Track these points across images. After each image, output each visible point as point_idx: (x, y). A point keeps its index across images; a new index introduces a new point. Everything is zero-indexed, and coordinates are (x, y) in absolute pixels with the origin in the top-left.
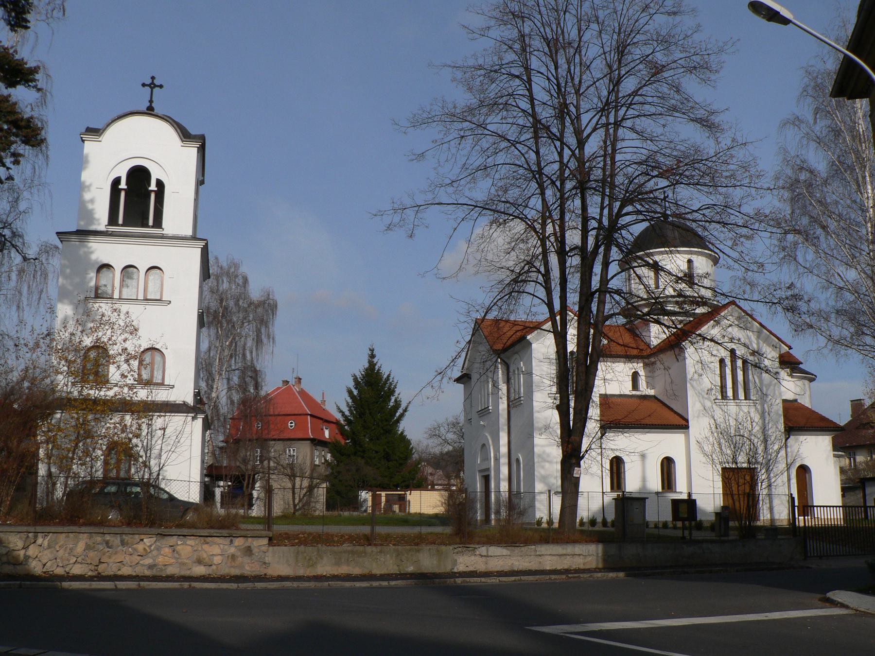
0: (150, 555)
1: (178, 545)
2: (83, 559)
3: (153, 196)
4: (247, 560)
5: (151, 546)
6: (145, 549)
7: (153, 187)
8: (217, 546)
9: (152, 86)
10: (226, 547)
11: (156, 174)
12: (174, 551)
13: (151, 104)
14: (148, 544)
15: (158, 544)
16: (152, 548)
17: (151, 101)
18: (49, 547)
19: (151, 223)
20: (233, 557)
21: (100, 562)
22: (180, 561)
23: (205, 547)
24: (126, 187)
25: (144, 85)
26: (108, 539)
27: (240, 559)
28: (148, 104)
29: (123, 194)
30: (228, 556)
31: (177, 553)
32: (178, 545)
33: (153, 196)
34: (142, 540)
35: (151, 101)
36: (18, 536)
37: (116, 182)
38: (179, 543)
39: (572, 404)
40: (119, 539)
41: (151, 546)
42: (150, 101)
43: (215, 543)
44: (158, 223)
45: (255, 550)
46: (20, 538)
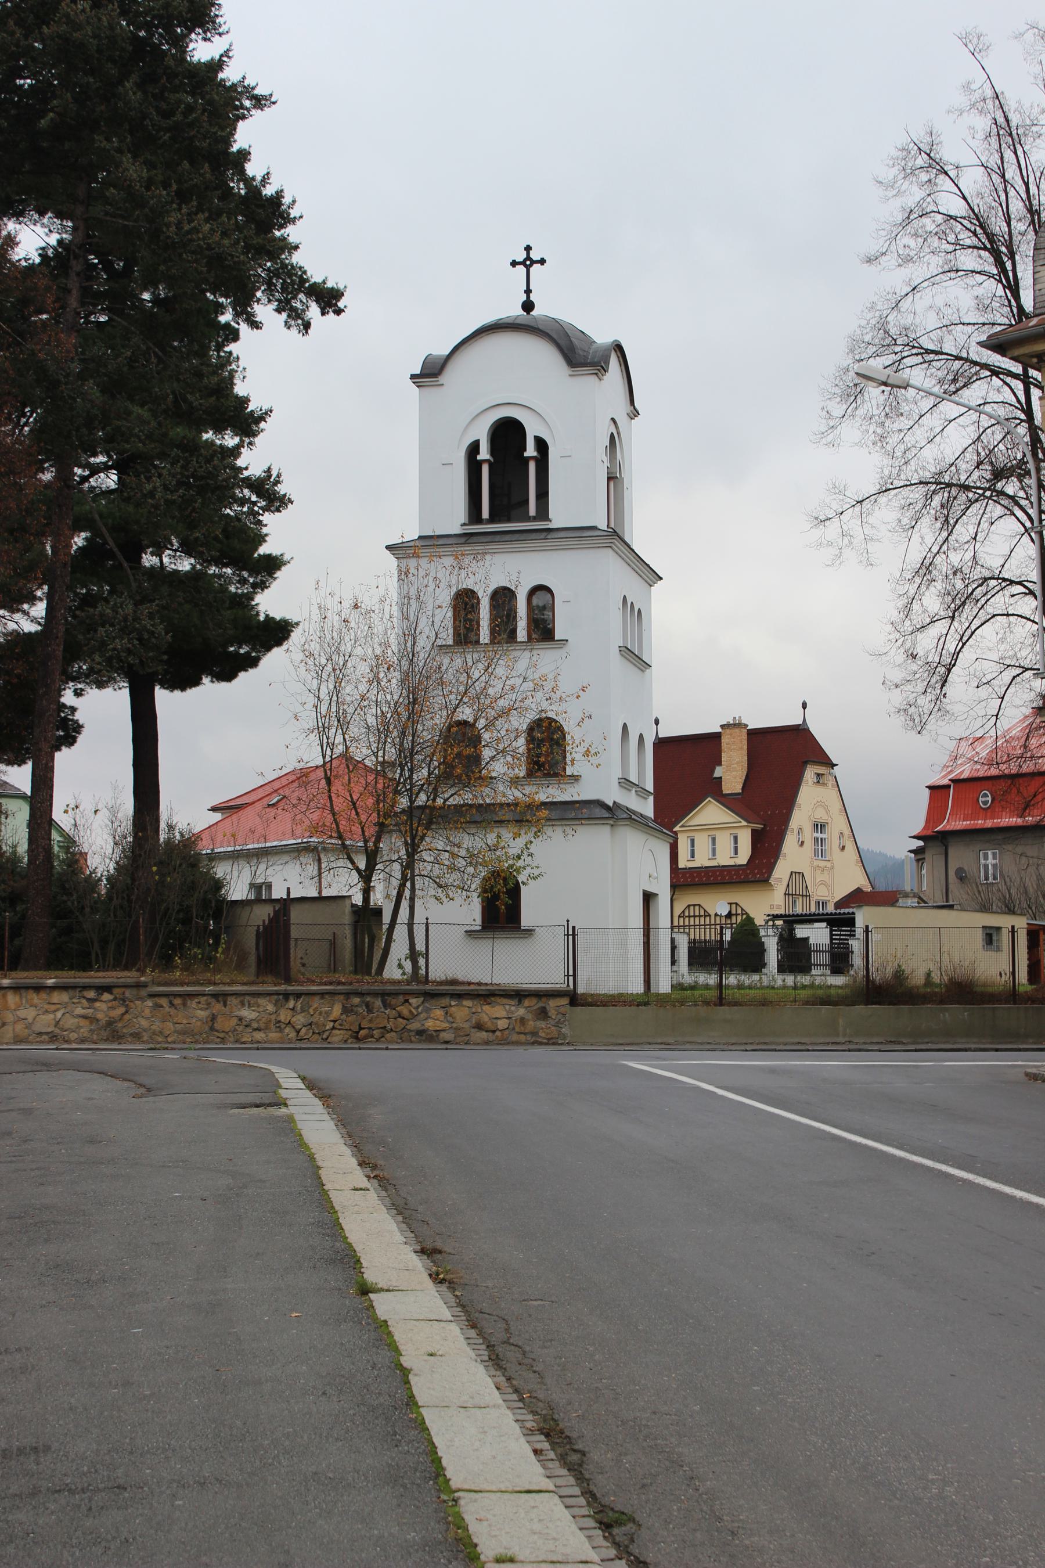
0: (418, 1018)
1: (451, 1006)
2: (341, 1025)
3: (532, 466)
4: (542, 1024)
5: (418, 1007)
6: (411, 1011)
7: (531, 451)
8: (502, 1007)
9: (528, 263)
10: (513, 1008)
11: (532, 430)
12: (446, 1013)
13: (528, 297)
14: (414, 1005)
15: (427, 1004)
16: (420, 1010)
17: (528, 291)
18: (303, 1011)
19: (532, 511)
20: (522, 1021)
21: (361, 1029)
22: (454, 1025)
23: (486, 1008)
24: (535, 454)
25: (514, 264)
26: (368, 1000)
27: (531, 1023)
28: (524, 297)
29: (485, 470)
30: (516, 1020)
31: (451, 1016)
32: (451, 1006)
33: (532, 466)
34: (407, 1001)
35: (528, 291)
36: (268, 998)
37: (474, 448)
38: (453, 1003)
39: (367, 940)
40: (380, 999)
41: (418, 1007)
42: (525, 292)
43: (499, 1004)
44: (543, 513)
45: (552, 1013)
46: (270, 1001)
